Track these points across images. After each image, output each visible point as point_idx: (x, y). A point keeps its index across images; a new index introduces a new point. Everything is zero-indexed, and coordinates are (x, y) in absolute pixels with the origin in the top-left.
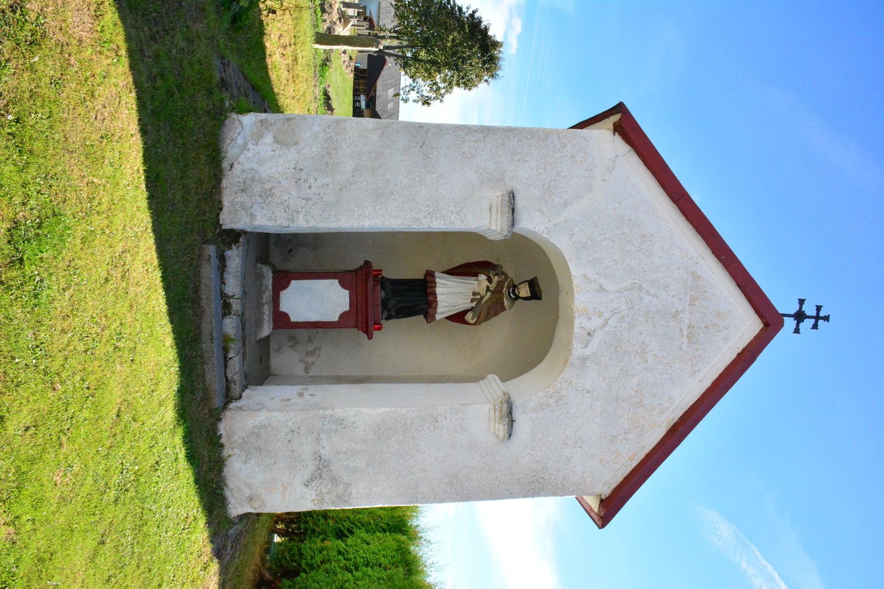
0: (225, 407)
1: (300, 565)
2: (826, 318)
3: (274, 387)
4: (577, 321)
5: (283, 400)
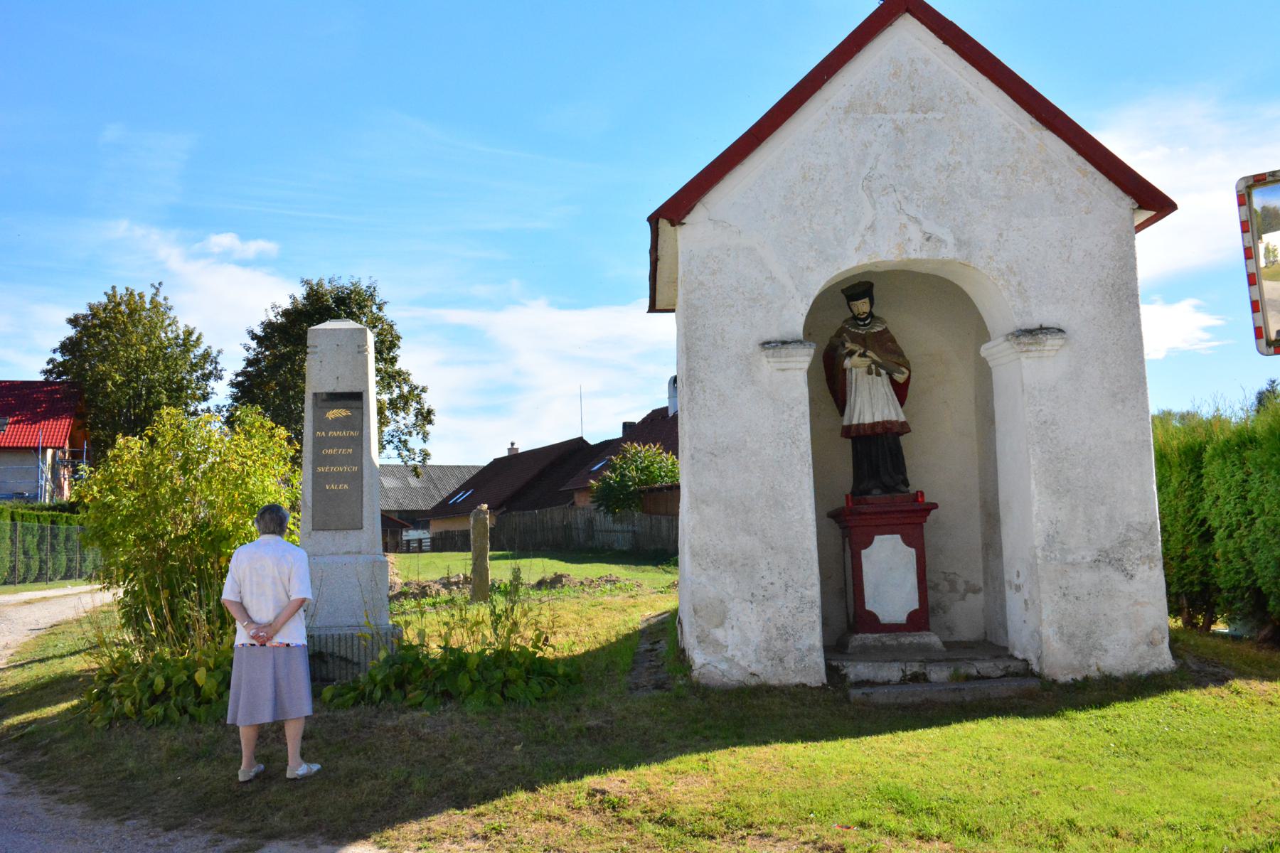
0: (1039, 676)
1: (1248, 588)
4: (913, 256)
5: (1027, 609)
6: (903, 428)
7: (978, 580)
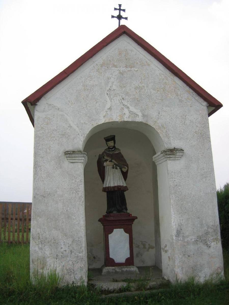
2: (120, 6)
3: (163, 264)
6: (125, 189)
7: (154, 245)
